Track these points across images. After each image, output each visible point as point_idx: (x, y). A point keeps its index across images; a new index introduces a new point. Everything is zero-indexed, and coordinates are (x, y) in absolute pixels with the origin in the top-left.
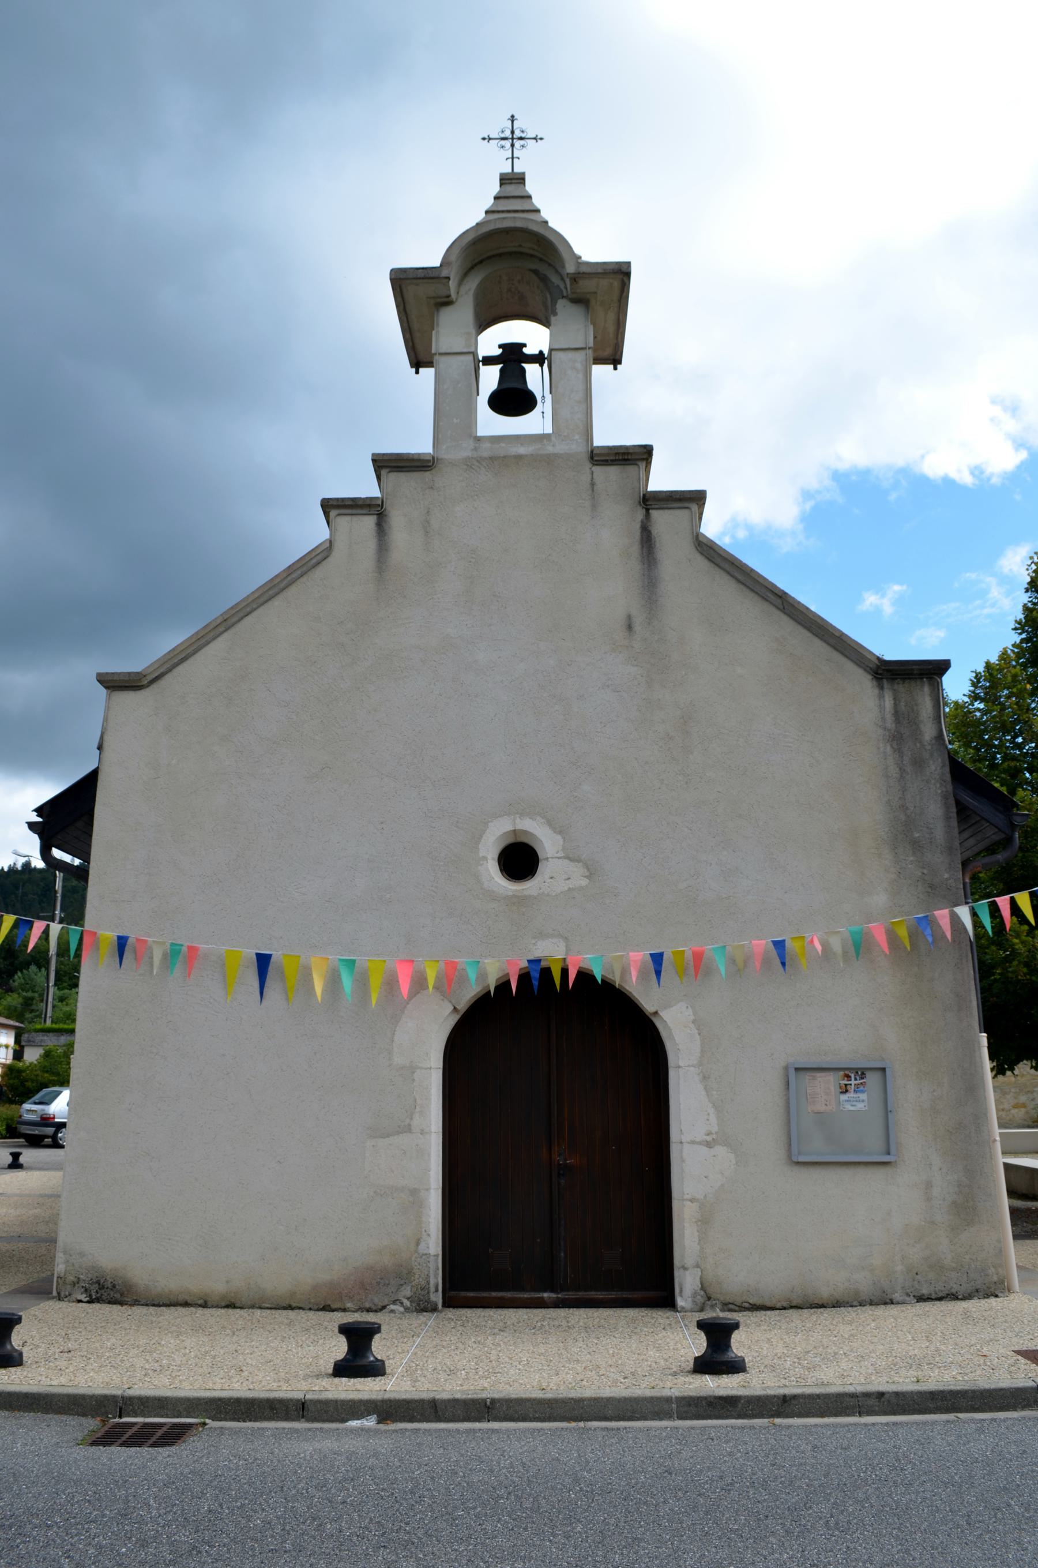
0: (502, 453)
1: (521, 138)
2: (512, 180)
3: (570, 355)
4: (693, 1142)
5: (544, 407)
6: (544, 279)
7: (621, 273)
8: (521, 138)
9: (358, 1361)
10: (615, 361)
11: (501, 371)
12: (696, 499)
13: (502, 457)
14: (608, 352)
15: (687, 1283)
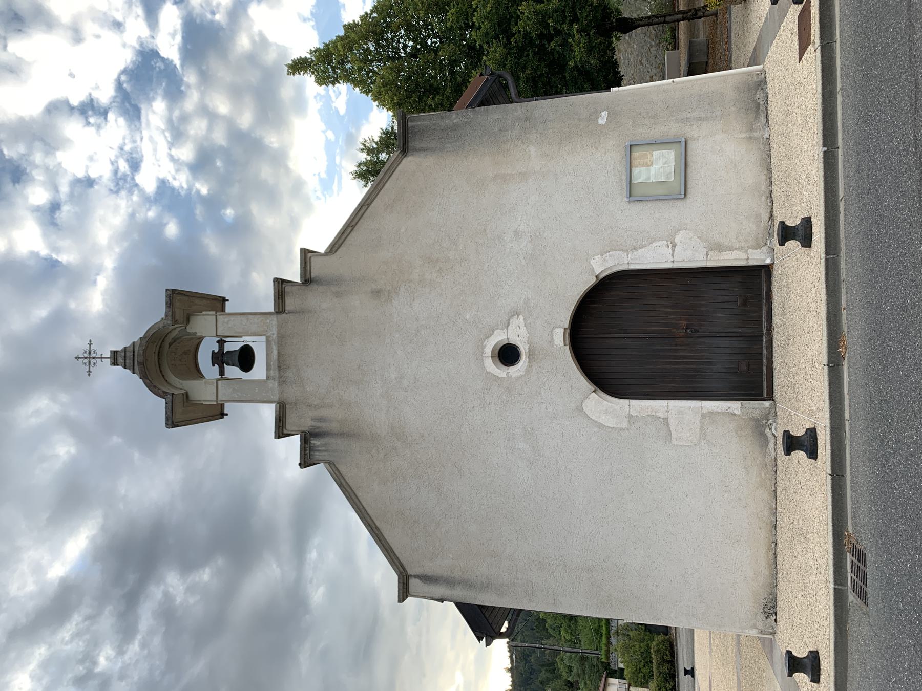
0: (276, 364)
1: (90, 353)
2: (115, 358)
3: (219, 325)
4: (673, 255)
5: (248, 340)
6: (175, 340)
7: (173, 296)
8: (90, 353)
9: (805, 444)
10: (224, 300)
11: (228, 365)
12: (306, 254)
13: (280, 366)
14: (219, 305)
15: (758, 257)
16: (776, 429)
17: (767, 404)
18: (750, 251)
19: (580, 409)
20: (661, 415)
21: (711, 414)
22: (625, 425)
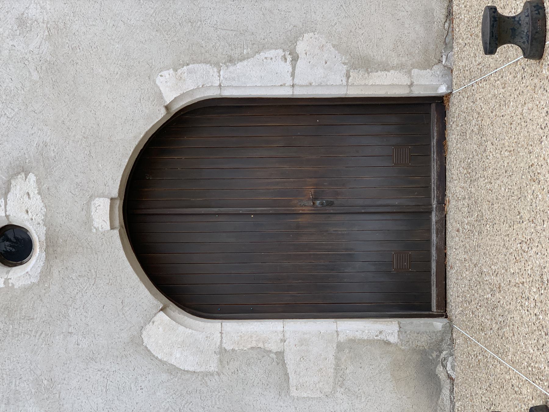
4: (293, 75)
15: (425, 83)
16: (453, 368)
17: (438, 324)
18: (415, 72)
19: (137, 342)
20: (274, 347)
21: (352, 345)
22: (213, 367)
